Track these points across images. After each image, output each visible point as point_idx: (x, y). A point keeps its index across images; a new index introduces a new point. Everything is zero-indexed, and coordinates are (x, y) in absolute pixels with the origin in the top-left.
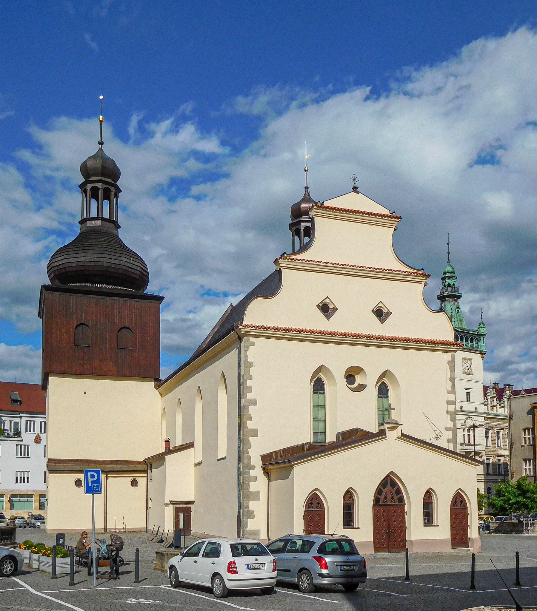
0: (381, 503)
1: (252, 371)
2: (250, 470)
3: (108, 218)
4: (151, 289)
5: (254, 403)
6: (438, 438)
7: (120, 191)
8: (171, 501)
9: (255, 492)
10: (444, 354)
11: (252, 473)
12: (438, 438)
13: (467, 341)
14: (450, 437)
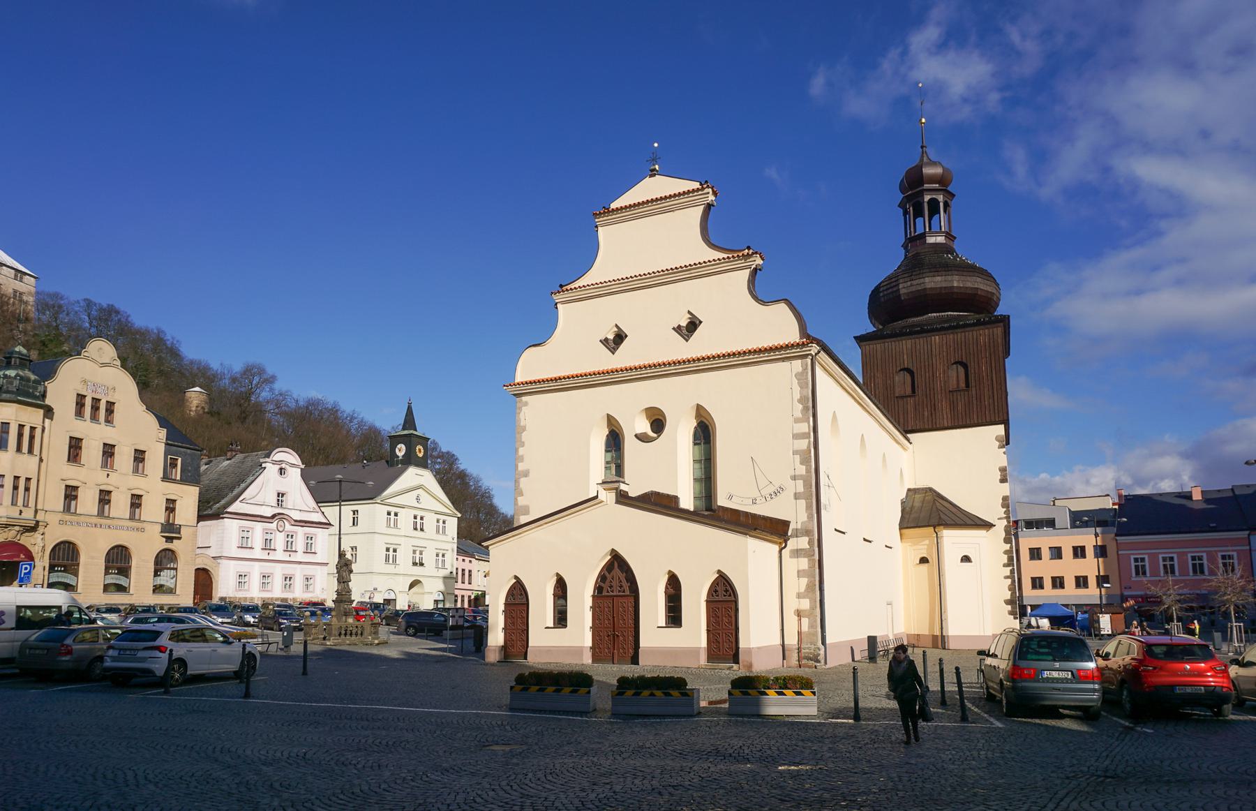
0: (605, 593)
4: (1001, 310)
6: (778, 494)
10: (786, 364)
12: (778, 494)
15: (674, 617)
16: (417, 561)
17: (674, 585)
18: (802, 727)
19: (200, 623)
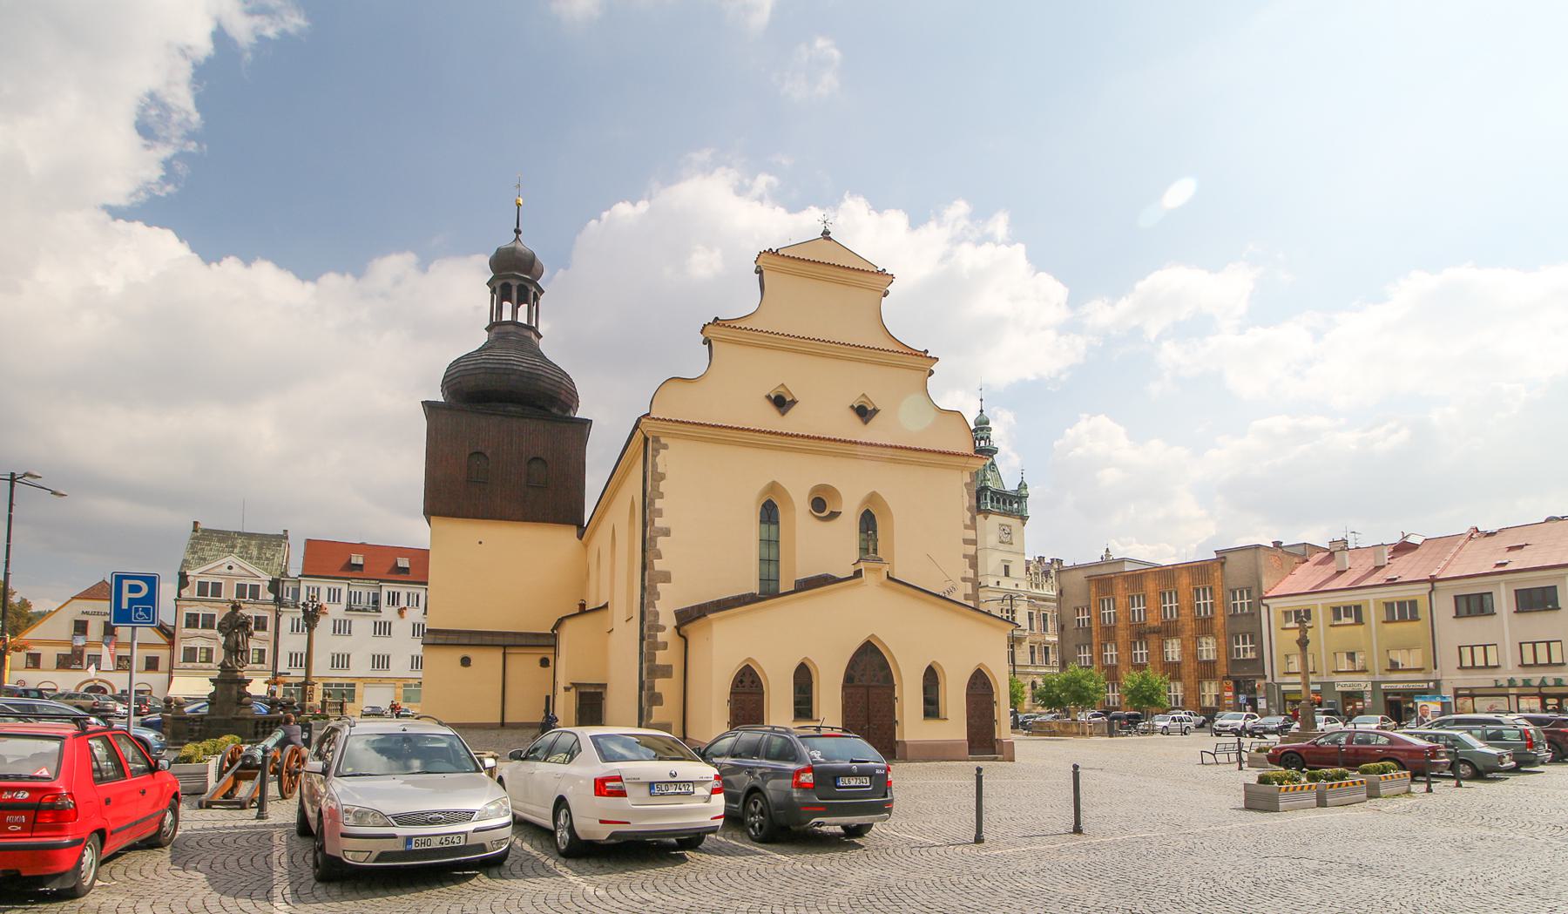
1: (663, 486)
2: (658, 631)
3: (526, 323)
5: (667, 532)
7: (542, 292)
8: (573, 684)
9: (664, 666)
11: (661, 637)
13: (1004, 503)
14: (970, 591)
15: (932, 708)
16: (279, 678)
17: (931, 678)
18: (259, 862)
19: (1550, 727)
